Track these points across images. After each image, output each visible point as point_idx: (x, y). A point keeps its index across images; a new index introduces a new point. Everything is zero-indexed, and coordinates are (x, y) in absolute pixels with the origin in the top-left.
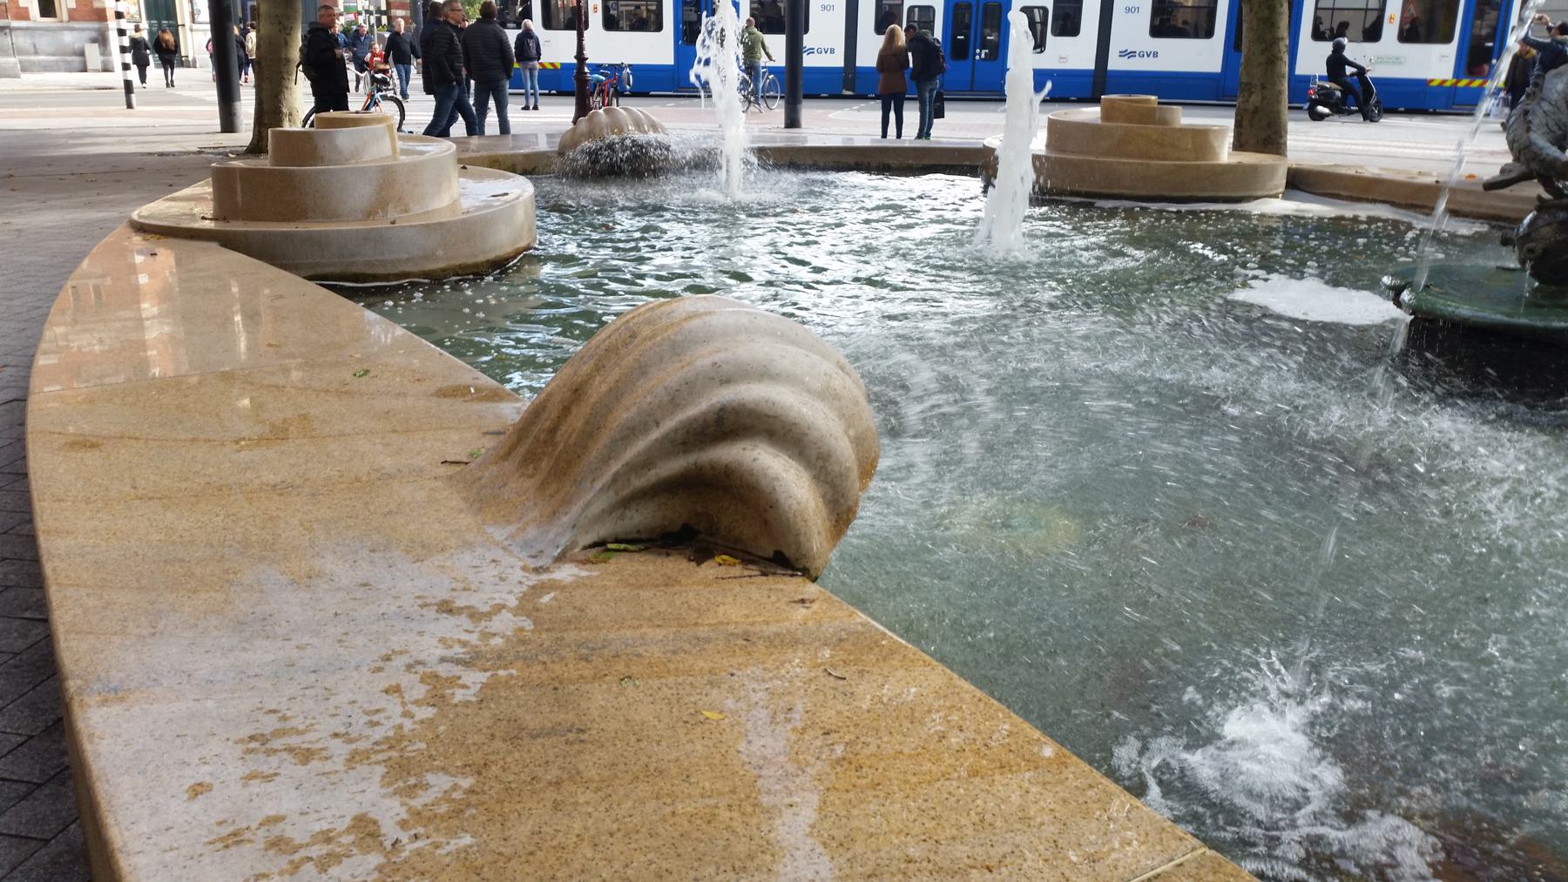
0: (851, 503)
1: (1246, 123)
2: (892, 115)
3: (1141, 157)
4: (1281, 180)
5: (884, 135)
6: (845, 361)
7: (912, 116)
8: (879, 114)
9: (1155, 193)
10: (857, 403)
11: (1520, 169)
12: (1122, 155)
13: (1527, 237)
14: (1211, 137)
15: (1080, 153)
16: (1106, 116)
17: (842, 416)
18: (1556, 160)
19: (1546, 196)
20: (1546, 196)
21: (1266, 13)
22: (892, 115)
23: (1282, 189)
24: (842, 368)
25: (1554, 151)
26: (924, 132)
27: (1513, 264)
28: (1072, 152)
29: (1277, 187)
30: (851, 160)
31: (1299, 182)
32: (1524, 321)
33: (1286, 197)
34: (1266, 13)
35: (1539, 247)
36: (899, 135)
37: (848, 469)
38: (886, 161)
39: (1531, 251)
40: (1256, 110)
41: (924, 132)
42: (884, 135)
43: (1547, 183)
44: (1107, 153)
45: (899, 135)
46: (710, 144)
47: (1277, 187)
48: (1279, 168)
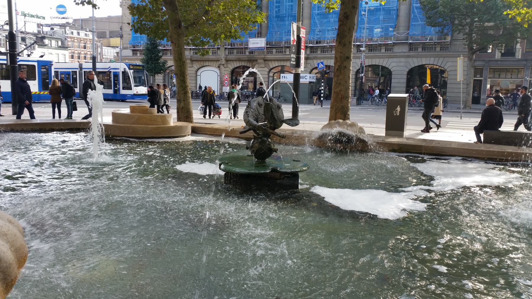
0: (12, 278)
1: (180, 111)
2: (56, 110)
3: (144, 125)
4: (190, 131)
5: (54, 117)
6: (11, 218)
7: (64, 110)
8: (51, 109)
9: (151, 136)
10: (15, 235)
11: (248, 128)
12: (139, 124)
13: (252, 147)
14: (167, 118)
15: (124, 123)
16: (133, 109)
17: (8, 242)
18: (256, 125)
19: (255, 135)
20: (255, 135)
21: (182, 78)
22: (56, 110)
23: (190, 133)
24: (10, 222)
25: (255, 123)
26: (70, 116)
27: (250, 153)
28: (121, 123)
29: (188, 132)
30: (37, 128)
31: (195, 131)
32: (253, 172)
33: (192, 135)
34: (182, 78)
35: (255, 149)
36: (60, 117)
37: (10, 264)
38: (52, 127)
39: (253, 151)
40: (183, 108)
41: (70, 116)
42: (54, 117)
43: (255, 131)
44: (133, 124)
45: (60, 117)
46: (105, 102)
47: (188, 132)
48: (190, 126)
